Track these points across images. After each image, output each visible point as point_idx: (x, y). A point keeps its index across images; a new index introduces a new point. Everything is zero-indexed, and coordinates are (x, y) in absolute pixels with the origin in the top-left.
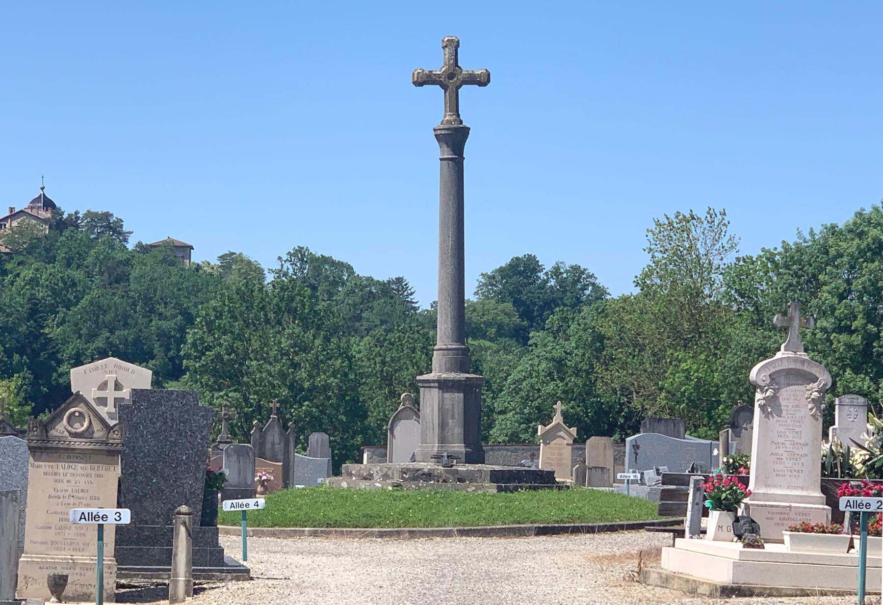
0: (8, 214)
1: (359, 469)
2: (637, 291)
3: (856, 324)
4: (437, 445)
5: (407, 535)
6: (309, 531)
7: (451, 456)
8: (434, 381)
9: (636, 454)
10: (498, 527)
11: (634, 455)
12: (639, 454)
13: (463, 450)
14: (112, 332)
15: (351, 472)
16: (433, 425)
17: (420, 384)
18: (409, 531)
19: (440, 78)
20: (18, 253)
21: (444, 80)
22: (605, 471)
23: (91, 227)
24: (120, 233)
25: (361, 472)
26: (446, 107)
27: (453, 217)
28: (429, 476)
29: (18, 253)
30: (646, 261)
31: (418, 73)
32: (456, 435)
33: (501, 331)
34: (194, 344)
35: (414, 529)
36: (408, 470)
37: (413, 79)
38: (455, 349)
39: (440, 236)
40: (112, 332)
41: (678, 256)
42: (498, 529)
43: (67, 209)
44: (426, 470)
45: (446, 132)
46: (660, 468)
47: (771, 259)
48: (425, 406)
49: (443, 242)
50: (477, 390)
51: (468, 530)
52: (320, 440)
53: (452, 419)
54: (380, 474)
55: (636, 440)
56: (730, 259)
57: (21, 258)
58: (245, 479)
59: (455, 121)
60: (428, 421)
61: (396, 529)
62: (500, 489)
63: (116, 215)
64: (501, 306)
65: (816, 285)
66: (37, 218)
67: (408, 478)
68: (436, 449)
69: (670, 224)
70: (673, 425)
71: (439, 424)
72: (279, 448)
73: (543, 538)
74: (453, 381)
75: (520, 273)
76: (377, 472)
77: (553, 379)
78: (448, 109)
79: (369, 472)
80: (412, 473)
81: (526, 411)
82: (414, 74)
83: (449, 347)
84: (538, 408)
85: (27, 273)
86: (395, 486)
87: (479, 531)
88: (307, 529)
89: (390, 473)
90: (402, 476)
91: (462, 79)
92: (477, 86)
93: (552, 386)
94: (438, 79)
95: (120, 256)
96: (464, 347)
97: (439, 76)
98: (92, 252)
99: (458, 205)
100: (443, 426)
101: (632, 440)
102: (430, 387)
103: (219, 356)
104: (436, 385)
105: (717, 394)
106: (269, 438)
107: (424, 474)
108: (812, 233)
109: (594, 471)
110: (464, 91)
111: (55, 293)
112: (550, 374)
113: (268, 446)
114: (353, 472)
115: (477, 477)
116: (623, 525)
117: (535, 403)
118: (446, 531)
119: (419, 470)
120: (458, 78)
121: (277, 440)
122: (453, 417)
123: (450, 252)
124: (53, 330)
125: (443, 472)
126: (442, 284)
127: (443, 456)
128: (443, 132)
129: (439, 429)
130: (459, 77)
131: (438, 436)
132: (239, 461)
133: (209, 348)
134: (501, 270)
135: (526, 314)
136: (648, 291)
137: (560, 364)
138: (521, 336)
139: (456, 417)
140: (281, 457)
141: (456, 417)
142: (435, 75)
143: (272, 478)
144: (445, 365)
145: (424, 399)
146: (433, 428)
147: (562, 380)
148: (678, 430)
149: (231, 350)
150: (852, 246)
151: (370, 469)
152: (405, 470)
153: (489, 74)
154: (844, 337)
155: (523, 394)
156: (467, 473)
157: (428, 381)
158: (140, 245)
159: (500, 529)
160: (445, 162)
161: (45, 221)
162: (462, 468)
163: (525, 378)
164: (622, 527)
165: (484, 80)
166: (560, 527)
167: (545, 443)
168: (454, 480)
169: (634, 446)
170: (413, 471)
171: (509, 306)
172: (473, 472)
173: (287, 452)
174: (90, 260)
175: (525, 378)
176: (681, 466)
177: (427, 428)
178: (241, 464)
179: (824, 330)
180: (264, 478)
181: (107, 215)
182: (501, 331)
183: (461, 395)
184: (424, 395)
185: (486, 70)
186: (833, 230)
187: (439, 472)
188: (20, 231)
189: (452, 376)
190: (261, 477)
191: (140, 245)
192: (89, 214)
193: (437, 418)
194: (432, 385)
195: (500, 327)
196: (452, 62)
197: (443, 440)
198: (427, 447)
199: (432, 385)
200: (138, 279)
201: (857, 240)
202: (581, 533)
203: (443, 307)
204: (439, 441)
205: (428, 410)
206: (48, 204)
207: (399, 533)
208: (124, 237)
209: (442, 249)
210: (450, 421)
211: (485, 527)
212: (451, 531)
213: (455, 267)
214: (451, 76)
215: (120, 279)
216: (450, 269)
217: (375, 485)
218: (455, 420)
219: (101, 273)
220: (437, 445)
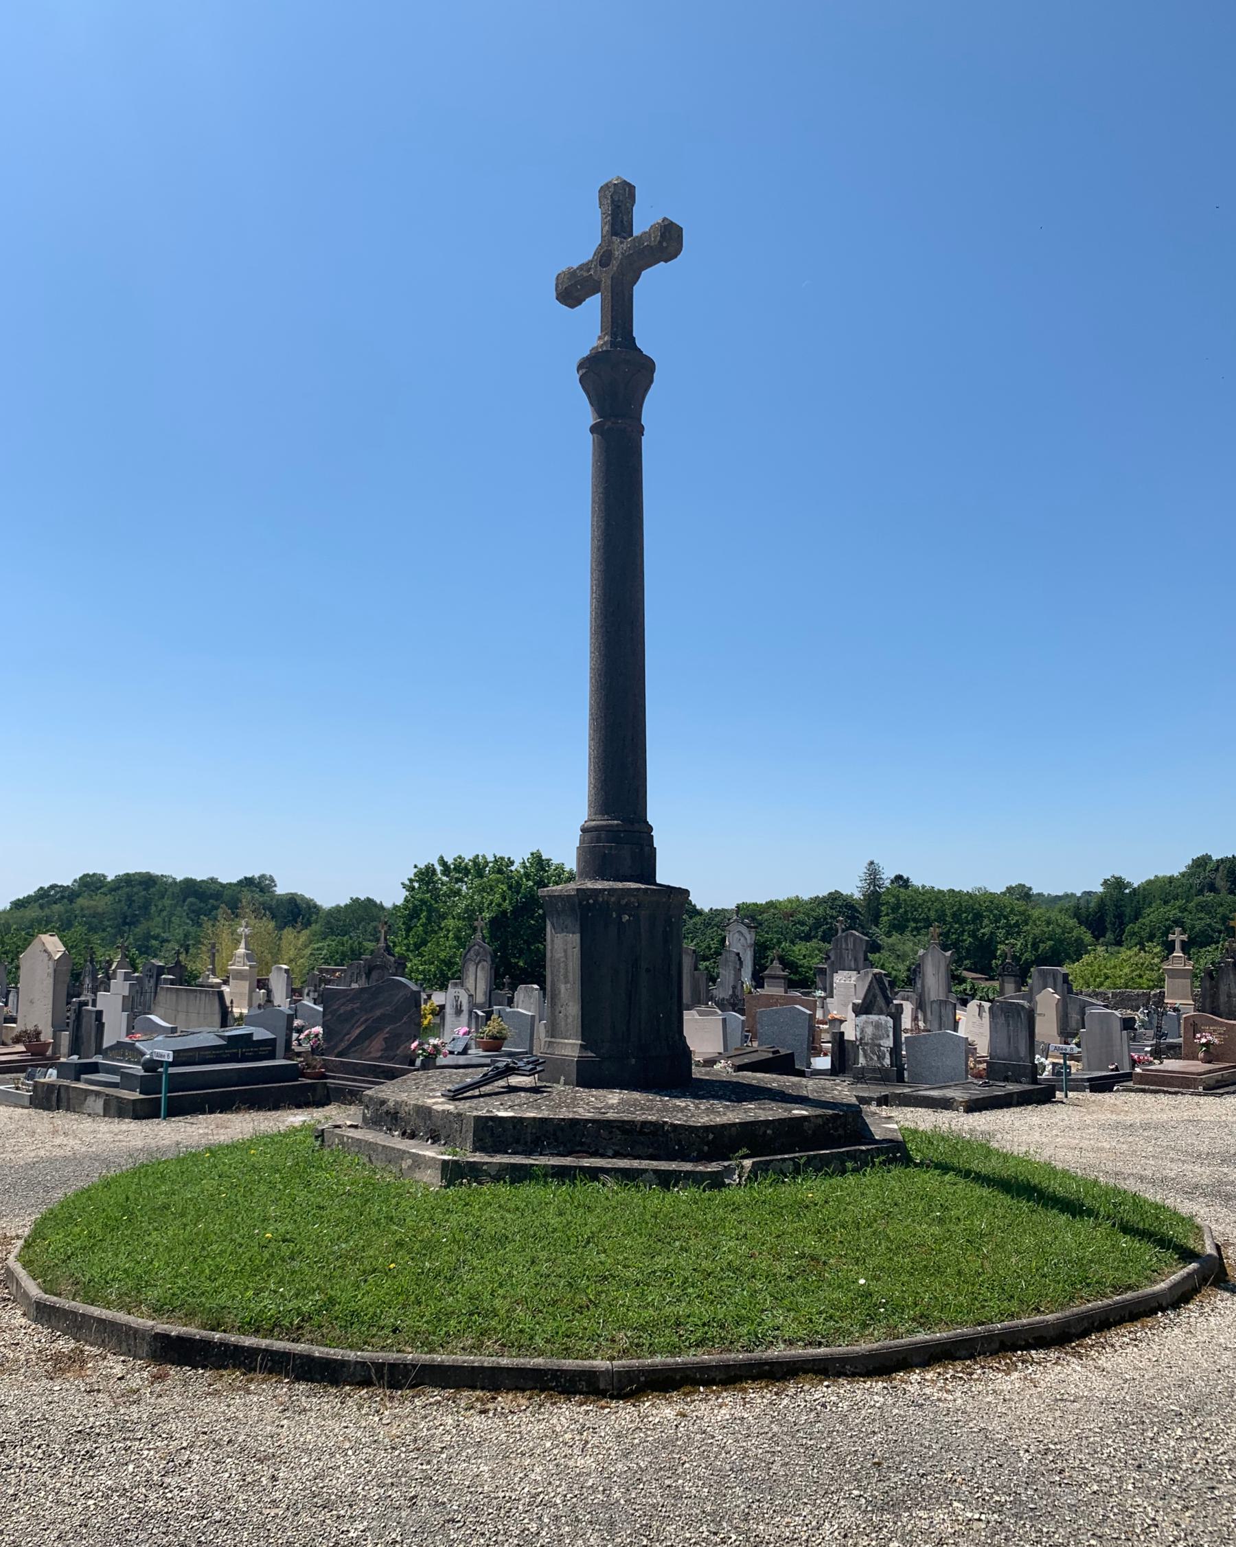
58: (1017, 1048)
94: (585, 274)
132: (1009, 1025)
178: (1011, 1028)
210: (563, 988)
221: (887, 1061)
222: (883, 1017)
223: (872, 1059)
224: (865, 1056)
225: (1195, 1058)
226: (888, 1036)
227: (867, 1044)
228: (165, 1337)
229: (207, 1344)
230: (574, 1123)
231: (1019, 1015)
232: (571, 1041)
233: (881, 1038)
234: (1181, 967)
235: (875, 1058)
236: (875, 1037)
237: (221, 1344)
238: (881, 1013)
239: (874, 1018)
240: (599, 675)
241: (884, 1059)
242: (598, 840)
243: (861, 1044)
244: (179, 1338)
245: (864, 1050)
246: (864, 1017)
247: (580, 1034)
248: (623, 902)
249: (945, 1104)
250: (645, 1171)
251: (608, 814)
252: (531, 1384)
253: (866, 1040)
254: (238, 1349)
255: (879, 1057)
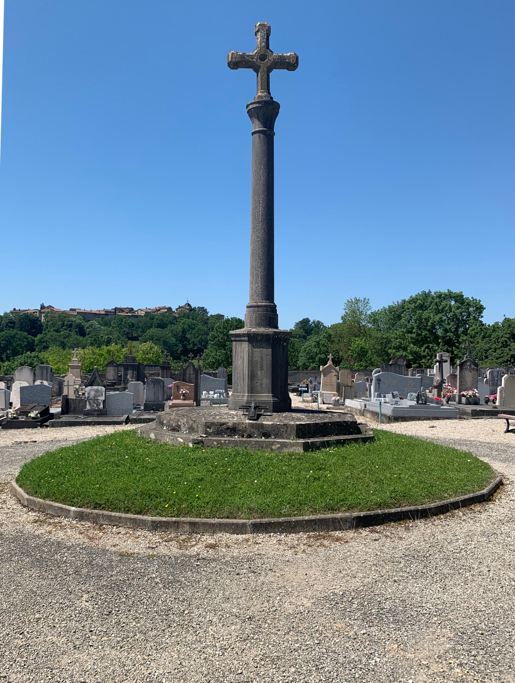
0: (178, 307)
1: (169, 419)
2: (341, 322)
3: (414, 331)
4: (247, 394)
5: (187, 528)
6: (75, 512)
7: (259, 406)
8: (244, 335)
9: (379, 384)
10: (306, 518)
11: (378, 384)
12: (381, 384)
13: (271, 399)
14: (202, 336)
15: (163, 421)
16: (244, 375)
17: (233, 339)
18: (190, 523)
19: (252, 59)
20: (181, 317)
21: (257, 60)
22: (352, 387)
23: (199, 310)
24: (206, 312)
25: (171, 422)
26: (258, 86)
27: (264, 185)
28: (233, 430)
29: (181, 317)
30: (343, 313)
31: (233, 53)
32: (264, 386)
33: (300, 337)
34: (212, 337)
35: (197, 520)
36: (212, 424)
37: (228, 60)
38: (265, 306)
39: (253, 197)
40: (202, 336)
41: (354, 312)
42: (306, 521)
43: (193, 306)
44: (230, 424)
45: (257, 105)
46: (394, 392)
47: (385, 310)
48: (237, 358)
49: (255, 208)
50: (285, 344)
51: (266, 523)
52: (222, 371)
53: (261, 370)
54: (187, 426)
55: (378, 376)
56: (369, 312)
57: (181, 318)
58: (158, 397)
59: (265, 96)
60: (239, 372)
61: (174, 519)
62: (307, 447)
63: (205, 308)
64: (300, 330)
65: (399, 317)
66: (185, 308)
67: (213, 432)
68: (245, 399)
69: (352, 302)
70: (398, 368)
71: (248, 376)
72: (193, 376)
73: (365, 532)
74: (262, 335)
75: (305, 323)
76: (184, 424)
77: (316, 347)
78: (260, 87)
79: (178, 424)
80: (216, 427)
81: (308, 357)
82: (228, 55)
83: (259, 304)
84: (311, 356)
85: (182, 321)
86: (195, 443)
87: (280, 524)
88: (73, 509)
89: (195, 426)
90: (206, 431)
91: (272, 60)
92: (286, 70)
93: (316, 350)
94: (250, 59)
95: (206, 318)
96: (273, 304)
97: (252, 57)
98: (199, 317)
99: (268, 176)
100: (252, 376)
101: (376, 376)
102: (241, 341)
103: (219, 340)
104: (246, 338)
105: (367, 352)
106: (188, 372)
107: (228, 428)
108: (398, 303)
109: (346, 387)
110: (275, 74)
111: (189, 326)
112: (315, 346)
113: (188, 376)
114: (165, 422)
115: (283, 431)
116: (457, 502)
117: (311, 355)
118: (237, 525)
119: (224, 424)
120: (269, 60)
121: (192, 373)
122: (262, 369)
123: (260, 217)
124: (188, 336)
125: (247, 427)
126: (254, 247)
127: (250, 407)
128: (254, 106)
129: (248, 378)
130: (270, 58)
131: (248, 387)
132: (155, 388)
133: (216, 337)
134: (300, 322)
135: (306, 332)
136: (344, 322)
137: (318, 343)
138: (305, 338)
139: (265, 368)
140: (194, 381)
141: (265, 368)
142: (248, 56)
143: (188, 392)
144: (255, 320)
145: (235, 351)
146: (244, 378)
147: (319, 348)
148: (402, 371)
149: (222, 338)
150: (413, 306)
151: (178, 421)
152: (209, 425)
153: (297, 58)
154: (410, 335)
155: (307, 352)
156: (272, 427)
157: (238, 335)
158: (211, 315)
159: (308, 521)
160: (256, 135)
161: (188, 309)
162: (267, 422)
163: (308, 347)
164: (456, 506)
165: (293, 60)
166: (385, 514)
167: (325, 375)
168: (259, 435)
169: (378, 380)
170: (217, 425)
171: (302, 330)
172: (279, 427)
173: (197, 378)
174: (198, 319)
175: (308, 347)
176: (404, 391)
177: (238, 379)
178: (156, 389)
179: (403, 332)
180: (184, 392)
181: (203, 308)
182: (300, 336)
183: (270, 350)
184: (236, 348)
185: (295, 54)
186: (404, 301)
187: (243, 426)
188: (181, 311)
189: (262, 330)
190: (182, 391)
191: (211, 315)
192: (199, 307)
193: (247, 369)
194: (243, 339)
195: (300, 335)
196: (263, 44)
197: (252, 390)
198: (238, 396)
199: (243, 339)
200: (211, 323)
201: (414, 304)
202: (410, 519)
203: (254, 268)
204: (248, 391)
205: (239, 362)
206: (189, 305)
207: (177, 525)
208: (207, 313)
209: (253, 215)
210: (259, 373)
211: (289, 519)
212: (244, 524)
213: (265, 231)
214: (263, 57)
215: (206, 323)
216: (261, 234)
217: (177, 440)
218: (263, 372)
219: (201, 322)
220: (247, 394)
221: (101, 406)
222: (100, 387)
223: (93, 406)
224: (90, 404)
225: (179, 399)
226: (102, 395)
227: (91, 399)
228: (359, 517)
229: (377, 516)
230: (325, 423)
231: (160, 383)
232: (264, 394)
233: (98, 397)
234: (76, 364)
235: (95, 405)
236: (95, 396)
237: (383, 514)
238: (99, 385)
239: (95, 387)
240: (264, 240)
241: (99, 405)
242: (267, 311)
243: (88, 400)
244: (364, 516)
245: (89, 402)
246: (89, 388)
247: (270, 390)
248: (285, 338)
249: (120, 423)
250: (359, 438)
251: (268, 300)
252: (472, 502)
253: (91, 398)
254: (390, 514)
255: (97, 405)
